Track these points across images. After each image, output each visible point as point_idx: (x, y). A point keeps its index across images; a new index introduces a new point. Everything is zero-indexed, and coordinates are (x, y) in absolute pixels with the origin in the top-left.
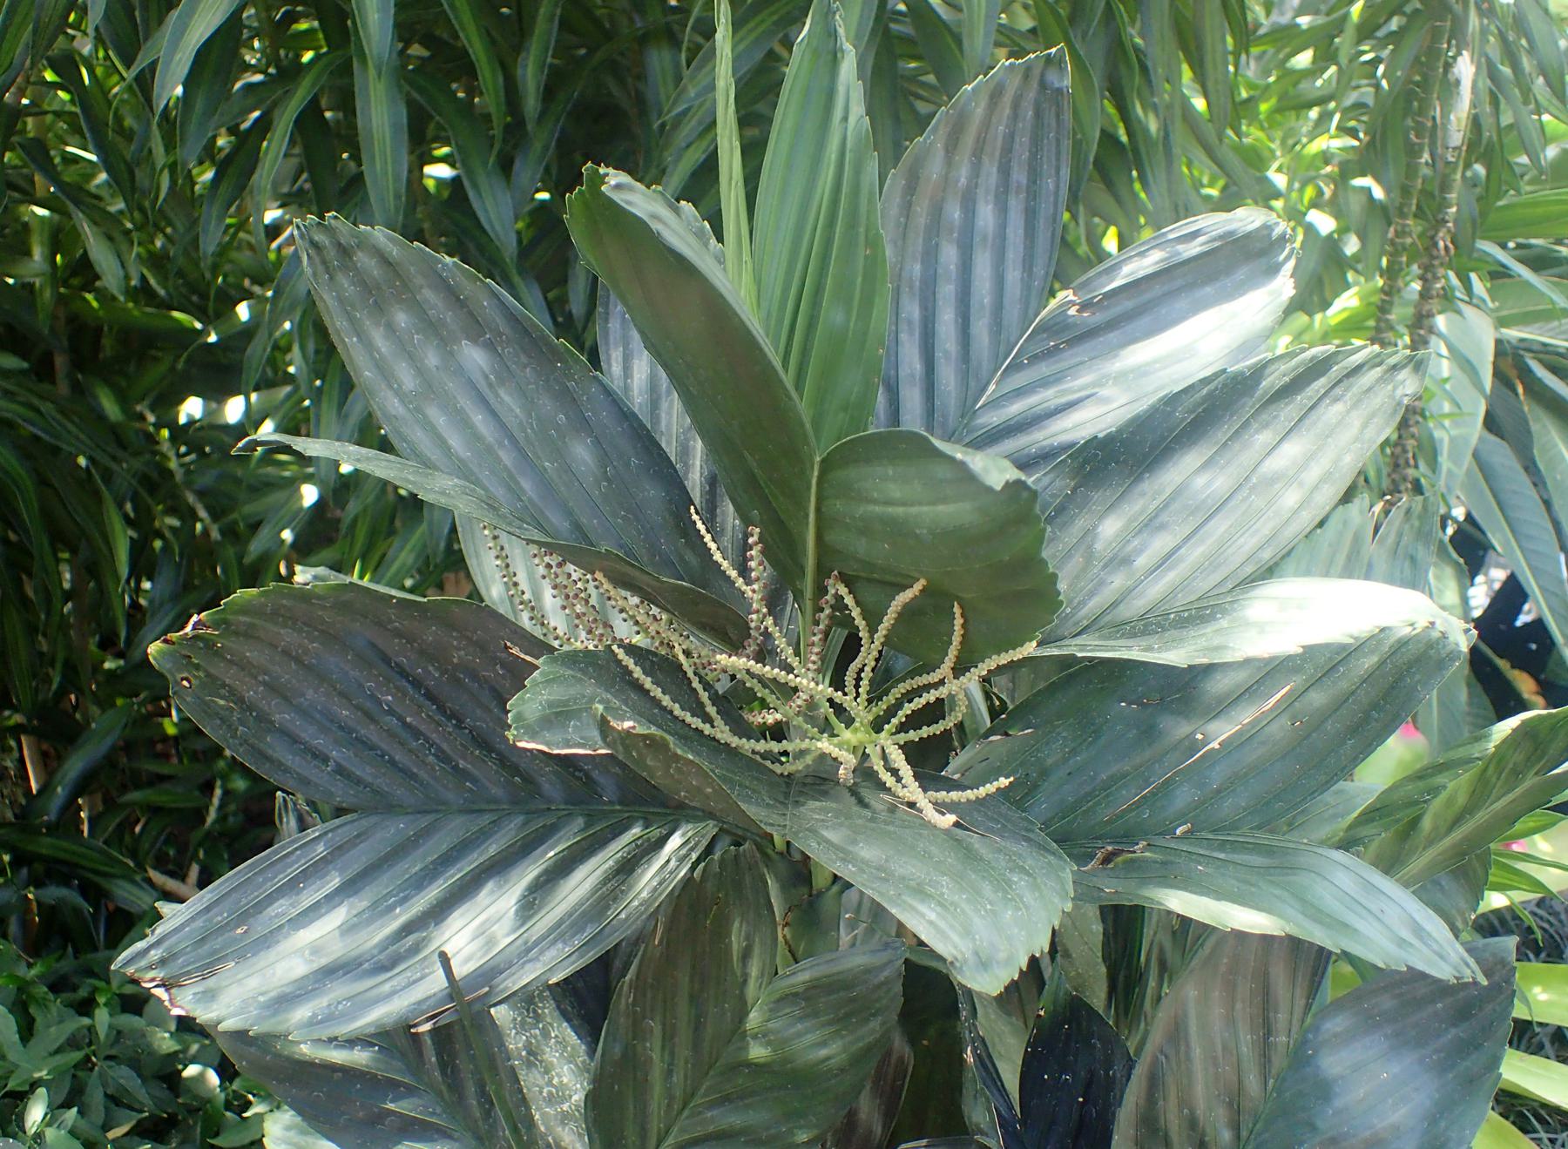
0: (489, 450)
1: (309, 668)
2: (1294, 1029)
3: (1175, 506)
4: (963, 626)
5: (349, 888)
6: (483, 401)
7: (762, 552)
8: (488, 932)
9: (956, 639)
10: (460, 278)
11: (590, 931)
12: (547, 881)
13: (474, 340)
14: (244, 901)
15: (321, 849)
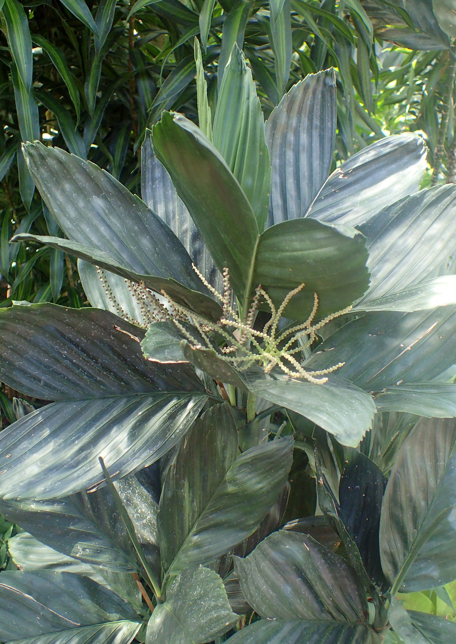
0: (108, 241)
1: (29, 341)
2: (446, 459)
3: (391, 252)
4: (318, 303)
5: (54, 434)
6: (104, 221)
7: (229, 280)
8: (118, 448)
9: (315, 308)
10: (91, 168)
11: (160, 444)
12: (139, 425)
13: (98, 196)
14: (8, 443)
15: (40, 419)
